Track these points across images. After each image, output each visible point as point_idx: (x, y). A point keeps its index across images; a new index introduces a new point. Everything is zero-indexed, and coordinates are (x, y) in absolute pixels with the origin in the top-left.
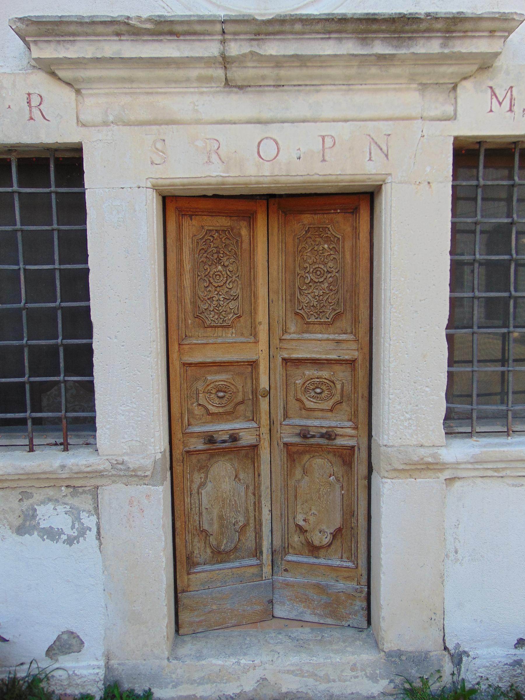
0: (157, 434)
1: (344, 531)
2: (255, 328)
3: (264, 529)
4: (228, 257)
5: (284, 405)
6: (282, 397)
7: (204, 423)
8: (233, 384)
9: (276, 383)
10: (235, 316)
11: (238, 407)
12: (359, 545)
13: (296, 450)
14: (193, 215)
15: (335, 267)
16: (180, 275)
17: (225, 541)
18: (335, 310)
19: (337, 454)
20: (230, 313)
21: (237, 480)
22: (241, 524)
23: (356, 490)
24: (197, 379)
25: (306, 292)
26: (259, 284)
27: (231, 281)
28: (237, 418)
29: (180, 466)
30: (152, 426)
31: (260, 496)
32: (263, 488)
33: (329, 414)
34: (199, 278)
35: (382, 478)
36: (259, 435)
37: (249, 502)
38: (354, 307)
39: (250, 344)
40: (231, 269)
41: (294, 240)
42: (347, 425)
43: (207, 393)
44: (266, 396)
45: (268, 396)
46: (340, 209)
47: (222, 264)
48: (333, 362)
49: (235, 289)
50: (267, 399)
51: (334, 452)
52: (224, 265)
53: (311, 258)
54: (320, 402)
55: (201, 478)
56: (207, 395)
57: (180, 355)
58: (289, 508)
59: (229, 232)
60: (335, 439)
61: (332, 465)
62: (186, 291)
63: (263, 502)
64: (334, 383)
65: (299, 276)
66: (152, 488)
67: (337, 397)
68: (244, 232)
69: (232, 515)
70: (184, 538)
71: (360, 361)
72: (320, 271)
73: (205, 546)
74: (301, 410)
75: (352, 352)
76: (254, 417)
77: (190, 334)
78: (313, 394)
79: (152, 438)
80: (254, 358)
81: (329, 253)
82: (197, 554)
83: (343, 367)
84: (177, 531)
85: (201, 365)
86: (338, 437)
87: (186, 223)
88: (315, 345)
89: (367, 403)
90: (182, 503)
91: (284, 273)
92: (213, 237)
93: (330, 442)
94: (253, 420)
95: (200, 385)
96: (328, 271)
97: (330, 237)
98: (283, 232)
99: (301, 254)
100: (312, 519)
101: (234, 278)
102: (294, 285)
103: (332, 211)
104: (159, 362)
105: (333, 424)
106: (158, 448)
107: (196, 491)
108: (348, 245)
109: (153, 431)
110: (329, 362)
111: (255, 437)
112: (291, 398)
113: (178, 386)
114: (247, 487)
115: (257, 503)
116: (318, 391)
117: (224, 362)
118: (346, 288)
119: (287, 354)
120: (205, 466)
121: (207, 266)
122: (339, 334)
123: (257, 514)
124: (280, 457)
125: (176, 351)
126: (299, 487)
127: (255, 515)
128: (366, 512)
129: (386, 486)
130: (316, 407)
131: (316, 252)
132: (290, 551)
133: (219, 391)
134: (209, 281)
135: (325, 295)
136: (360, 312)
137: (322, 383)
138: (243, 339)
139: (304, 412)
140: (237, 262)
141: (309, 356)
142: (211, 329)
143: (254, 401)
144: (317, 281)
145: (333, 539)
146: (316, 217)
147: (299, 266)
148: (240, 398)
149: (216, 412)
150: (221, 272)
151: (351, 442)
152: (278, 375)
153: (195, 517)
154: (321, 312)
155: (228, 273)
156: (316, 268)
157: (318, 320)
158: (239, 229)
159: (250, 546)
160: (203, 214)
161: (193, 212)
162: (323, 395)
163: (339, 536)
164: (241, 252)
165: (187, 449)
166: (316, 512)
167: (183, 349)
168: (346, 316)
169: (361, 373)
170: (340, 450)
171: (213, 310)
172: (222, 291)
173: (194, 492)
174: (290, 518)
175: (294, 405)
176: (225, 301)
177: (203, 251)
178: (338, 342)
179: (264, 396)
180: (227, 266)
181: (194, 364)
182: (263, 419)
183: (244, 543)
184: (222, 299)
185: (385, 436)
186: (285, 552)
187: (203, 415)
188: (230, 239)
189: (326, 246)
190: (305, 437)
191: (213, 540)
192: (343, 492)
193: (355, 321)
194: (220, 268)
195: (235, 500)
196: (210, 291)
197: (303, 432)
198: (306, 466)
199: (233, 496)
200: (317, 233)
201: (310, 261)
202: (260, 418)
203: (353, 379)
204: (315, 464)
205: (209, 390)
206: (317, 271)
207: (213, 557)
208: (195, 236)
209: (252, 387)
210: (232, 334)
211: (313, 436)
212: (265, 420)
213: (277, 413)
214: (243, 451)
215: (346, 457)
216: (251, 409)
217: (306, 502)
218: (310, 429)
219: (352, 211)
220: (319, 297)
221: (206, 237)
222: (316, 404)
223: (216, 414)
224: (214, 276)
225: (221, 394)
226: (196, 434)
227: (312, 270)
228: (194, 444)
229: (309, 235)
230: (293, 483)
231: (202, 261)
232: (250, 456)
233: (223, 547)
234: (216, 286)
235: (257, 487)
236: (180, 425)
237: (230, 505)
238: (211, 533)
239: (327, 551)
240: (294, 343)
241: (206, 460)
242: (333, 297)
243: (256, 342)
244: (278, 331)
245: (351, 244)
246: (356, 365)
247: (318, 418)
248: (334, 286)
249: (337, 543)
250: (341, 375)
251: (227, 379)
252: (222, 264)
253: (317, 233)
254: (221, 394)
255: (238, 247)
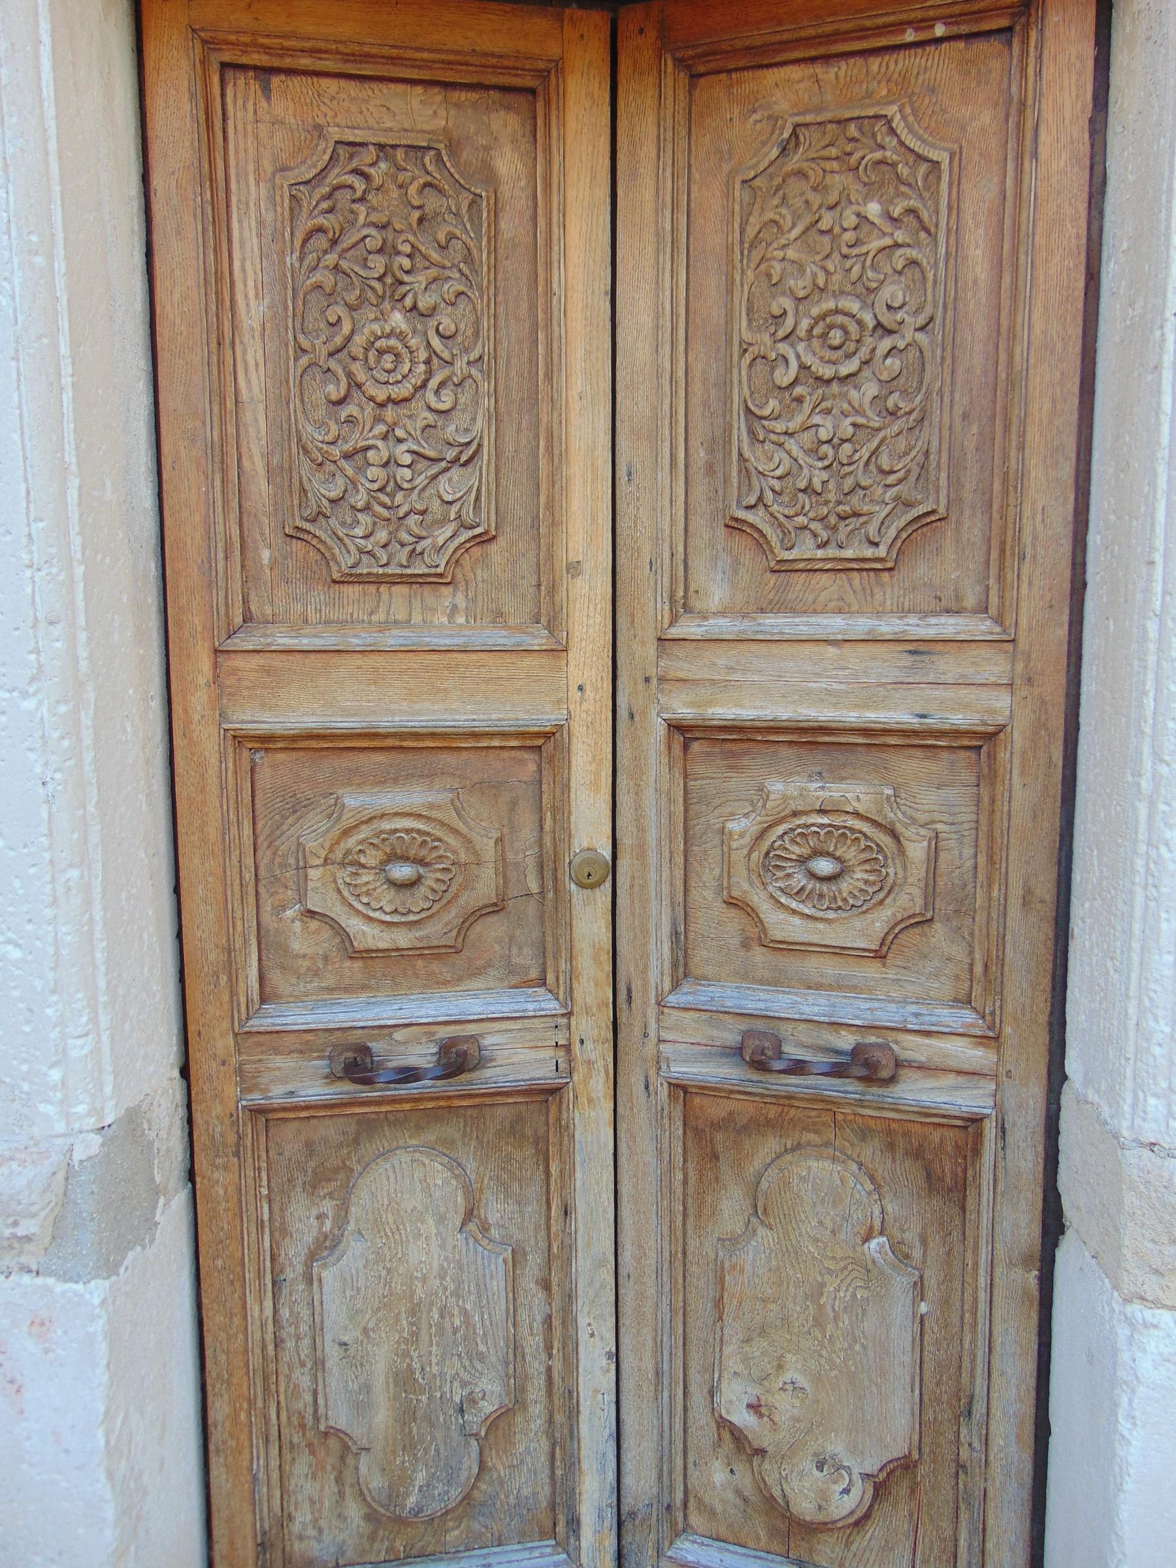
0: (78, 1049)
1: (922, 1470)
2: (553, 589)
3: (584, 1428)
4: (433, 272)
5: (674, 924)
6: (665, 889)
7: (331, 990)
8: (455, 831)
9: (642, 830)
10: (466, 535)
11: (478, 927)
12: (989, 1545)
13: (724, 1114)
14: (278, 71)
15: (913, 305)
16: (222, 339)
17: (421, 1477)
18: (909, 505)
19: (901, 1142)
20: (443, 521)
21: (472, 1226)
22: (488, 1407)
23: (983, 1307)
24: (297, 807)
25: (779, 427)
26: (574, 394)
27: (449, 378)
28: (476, 972)
29: (226, 1168)
30: (50, 1011)
31: (570, 1297)
32: (582, 1264)
33: (871, 971)
34: (304, 361)
35: (1127, 1301)
36: (568, 1048)
37: (523, 1315)
38: (997, 487)
39: (529, 661)
40: (447, 325)
41: (728, 194)
42: (947, 1020)
43: (343, 864)
44: (598, 884)
45: (608, 884)
46: (947, 20)
47: (408, 302)
48: (892, 741)
49: (467, 416)
50: (603, 896)
51: (890, 1133)
52: (414, 307)
53: (801, 269)
54: (831, 915)
55: (320, 1217)
56: (343, 875)
57: (220, 696)
58: (692, 1347)
59: (439, 159)
60: (892, 1080)
61: (878, 1188)
62: (248, 417)
63: (582, 1321)
64: (895, 836)
65: (748, 357)
66: (60, 1287)
67: (909, 899)
68: (508, 164)
69: (450, 1372)
70: (245, 1464)
71: (1018, 737)
72: (846, 332)
73: (341, 1493)
74: (746, 945)
75: (984, 693)
76: (547, 970)
77: (268, 610)
78: (799, 880)
79: (53, 1065)
80: (545, 716)
81: (888, 241)
82: (304, 1524)
83: (938, 766)
84: (216, 1436)
85: (314, 744)
86: (904, 1073)
87: (242, 98)
88: (815, 664)
89: (1048, 930)
90: (237, 1320)
91: (681, 347)
92: (366, 177)
93: (875, 1093)
94: (542, 982)
95: (313, 833)
96: (879, 325)
97: (894, 165)
98: (682, 161)
99: (756, 255)
100: (785, 1406)
101: (460, 366)
102: (727, 399)
103: (910, 36)
104: (86, 720)
105: (888, 1015)
106: (81, 1109)
107: (300, 1269)
108: (980, 194)
109: (54, 1034)
110: (875, 739)
111: (550, 1053)
112: (705, 895)
113: (213, 833)
114: (518, 1257)
115: (556, 1322)
116: (824, 866)
117: (416, 736)
118: (962, 401)
119: (691, 704)
120: (337, 1170)
121: (339, 310)
122: (925, 614)
123: (557, 1365)
124: (652, 1141)
125: (202, 681)
126: (734, 1267)
127: (549, 1369)
128: (1028, 1408)
129: (1154, 1343)
130: (815, 939)
131: (827, 239)
132: (695, 1520)
133: (394, 857)
134: (350, 375)
135: (861, 433)
136: (1027, 512)
137: (844, 835)
138: (499, 637)
139: (759, 955)
140: (474, 294)
141: (784, 713)
142: (358, 588)
143: (549, 904)
144: (827, 372)
145: (875, 1497)
146: (829, 74)
147: (750, 310)
148: (485, 887)
149: (382, 945)
150: (401, 337)
151: (970, 1099)
152: (649, 796)
153: (297, 1373)
154: (842, 518)
155: (436, 343)
156: (823, 317)
157: (831, 552)
158: (487, 149)
159: (526, 1492)
160: (320, 65)
161: (267, 49)
162: (845, 885)
163: (901, 1490)
164: (494, 251)
165: (256, 1099)
166: (802, 1381)
167: (234, 671)
168: (958, 530)
169: (1025, 794)
170: (916, 1128)
171: (367, 508)
172: (408, 422)
173: (289, 1274)
174: (693, 1388)
175: (716, 926)
176: (421, 465)
177: (321, 242)
178: (919, 648)
179: (588, 884)
180: (433, 311)
181: (283, 738)
182: (584, 979)
183: (501, 1483)
184: (407, 459)
185: (1152, 1101)
186: (673, 1525)
187: (326, 958)
188: (440, 191)
189: (873, 209)
190: (760, 1065)
191: (371, 1474)
192: (923, 1308)
193: (1003, 551)
194: (398, 319)
195: (465, 1313)
196: (351, 420)
197: (752, 1044)
198: (764, 1185)
199: (456, 1294)
200: (834, 152)
201: (800, 285)
202: (572, 975)
203: (984, 821)
204: (802, 1179)
205: (348, 852)
206: (831, 327)
207: (372, 1538)
208: (284, 169)
209: (541, 846)
210: (451, 616)
211: (798, 1068)
212: (592, 987)
213: (645, 956)
214: (500, 1112)
215: (946, 1160)
216: (536, 934)
217: (763, 1332)
218: (785, 1030)
219: (1004, 22)
220: (836, 448)
221: (333, 178)
222: (811, 924)
223: (384, 954)
224: (372, 355)
225: (402, 872)
226: (291, 1038)
227: (805, 324)
228: (284, 1081)
229: (795, 161)
230: (709, 1250)
231: (318, 287)
232: (529, 1132)
233: (411, 1501)
234: (381, 396)
235: (559, 1257)
236: (226, 997)
237: (441, 1330)
238: (364, 1443)
239: (848, 1545)
240: (722, 657)
241: (341, 1145)
242: (902, 445)
243: (559, 651)
244: (648, 606)
245: (995, 191)
246: (1003, 755)
247: (819, 987)
248: (905, 393)
249: (893, 1520)
250: (929, 800)
251: (431, 806)
252: (408, 302)
253: (834, 152)
254: (402, 872)
255: (477, 228)
